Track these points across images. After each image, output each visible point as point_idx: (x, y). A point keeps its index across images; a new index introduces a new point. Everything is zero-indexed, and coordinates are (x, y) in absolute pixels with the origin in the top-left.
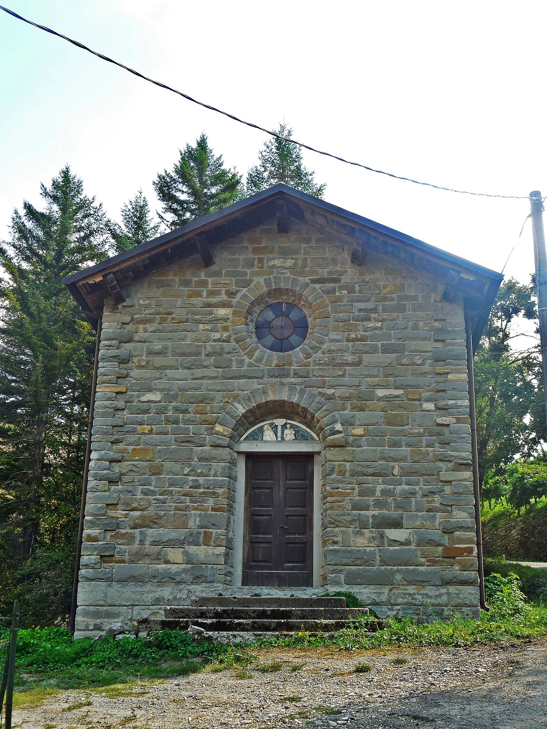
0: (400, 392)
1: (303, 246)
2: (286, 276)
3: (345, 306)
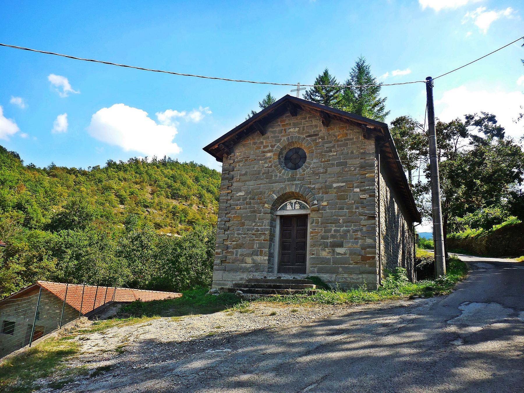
0: (344, 184)
1: (303, 121)
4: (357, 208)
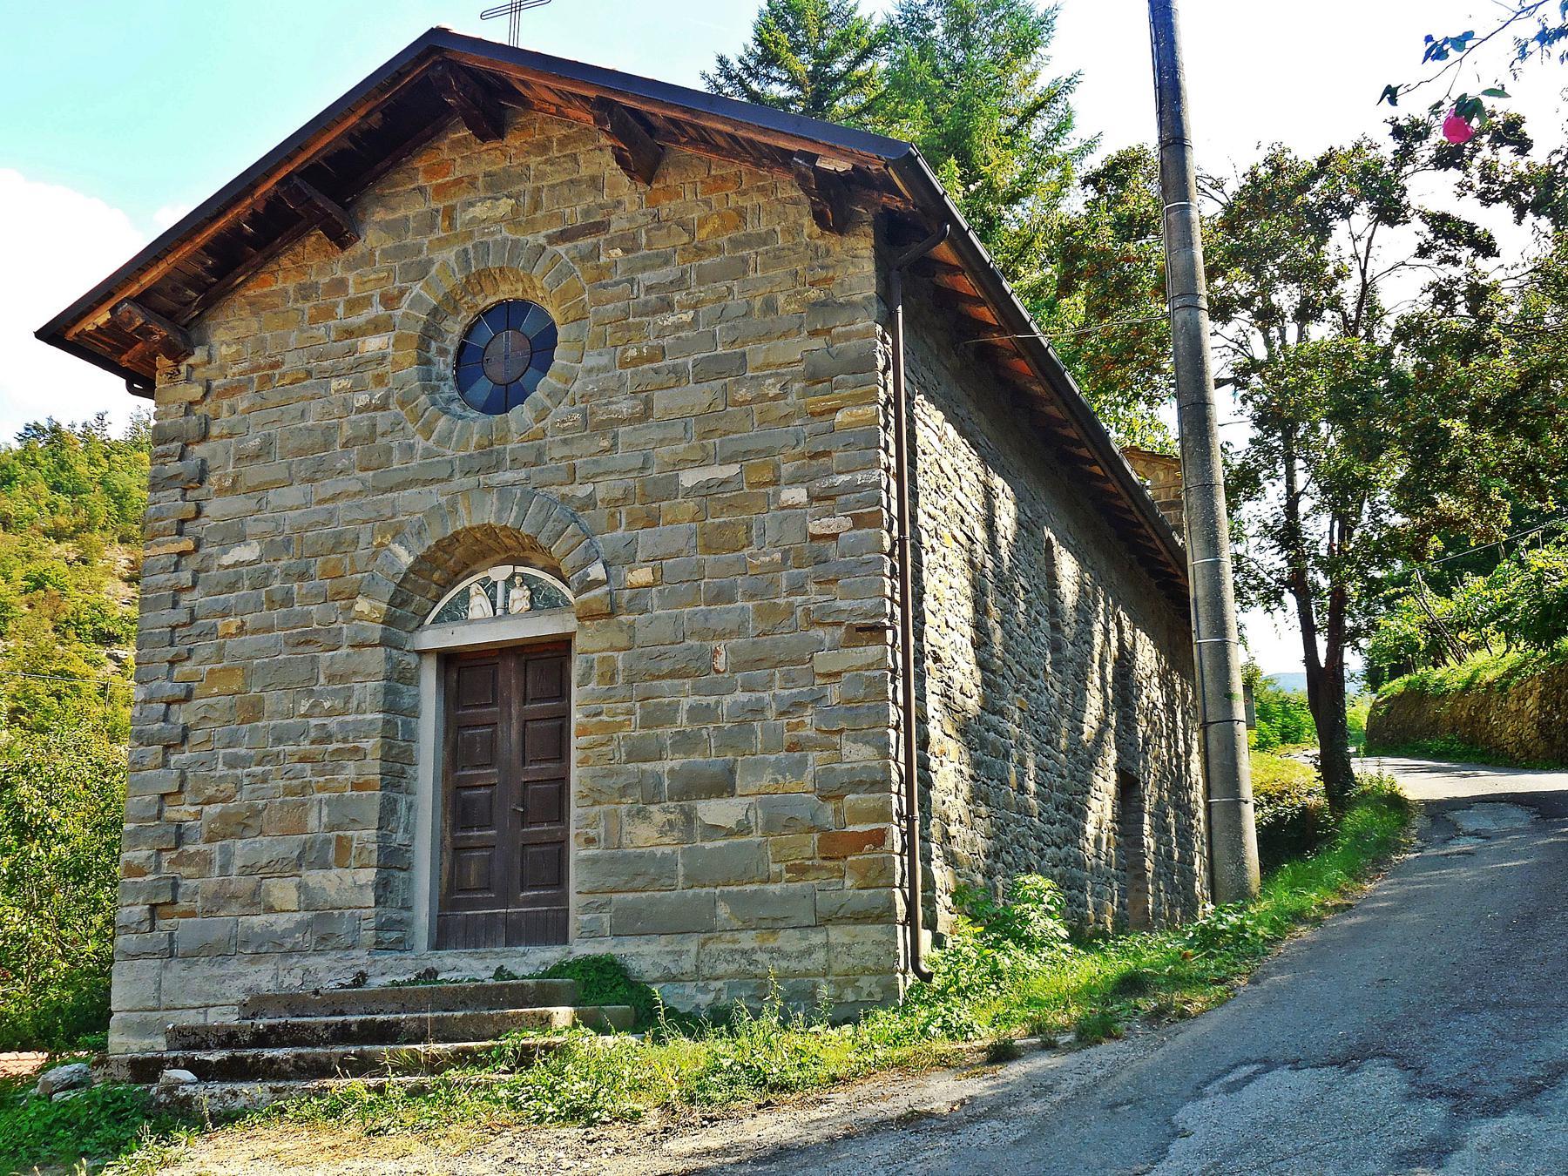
0: (734, 469)
1: (534, 161)
2: (498, 237)
3: (617, 284)
4: (797, 588)
